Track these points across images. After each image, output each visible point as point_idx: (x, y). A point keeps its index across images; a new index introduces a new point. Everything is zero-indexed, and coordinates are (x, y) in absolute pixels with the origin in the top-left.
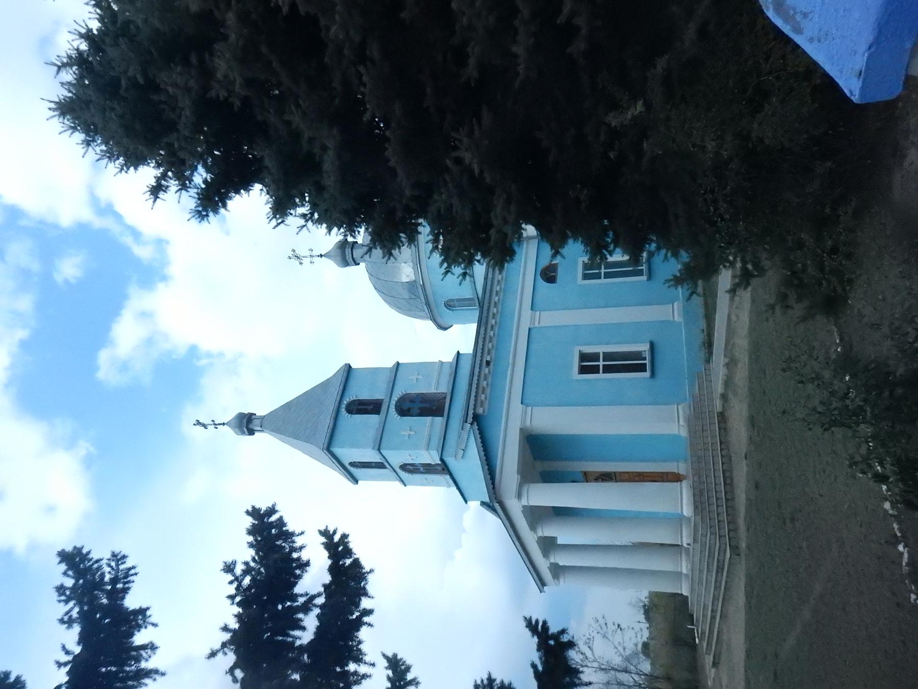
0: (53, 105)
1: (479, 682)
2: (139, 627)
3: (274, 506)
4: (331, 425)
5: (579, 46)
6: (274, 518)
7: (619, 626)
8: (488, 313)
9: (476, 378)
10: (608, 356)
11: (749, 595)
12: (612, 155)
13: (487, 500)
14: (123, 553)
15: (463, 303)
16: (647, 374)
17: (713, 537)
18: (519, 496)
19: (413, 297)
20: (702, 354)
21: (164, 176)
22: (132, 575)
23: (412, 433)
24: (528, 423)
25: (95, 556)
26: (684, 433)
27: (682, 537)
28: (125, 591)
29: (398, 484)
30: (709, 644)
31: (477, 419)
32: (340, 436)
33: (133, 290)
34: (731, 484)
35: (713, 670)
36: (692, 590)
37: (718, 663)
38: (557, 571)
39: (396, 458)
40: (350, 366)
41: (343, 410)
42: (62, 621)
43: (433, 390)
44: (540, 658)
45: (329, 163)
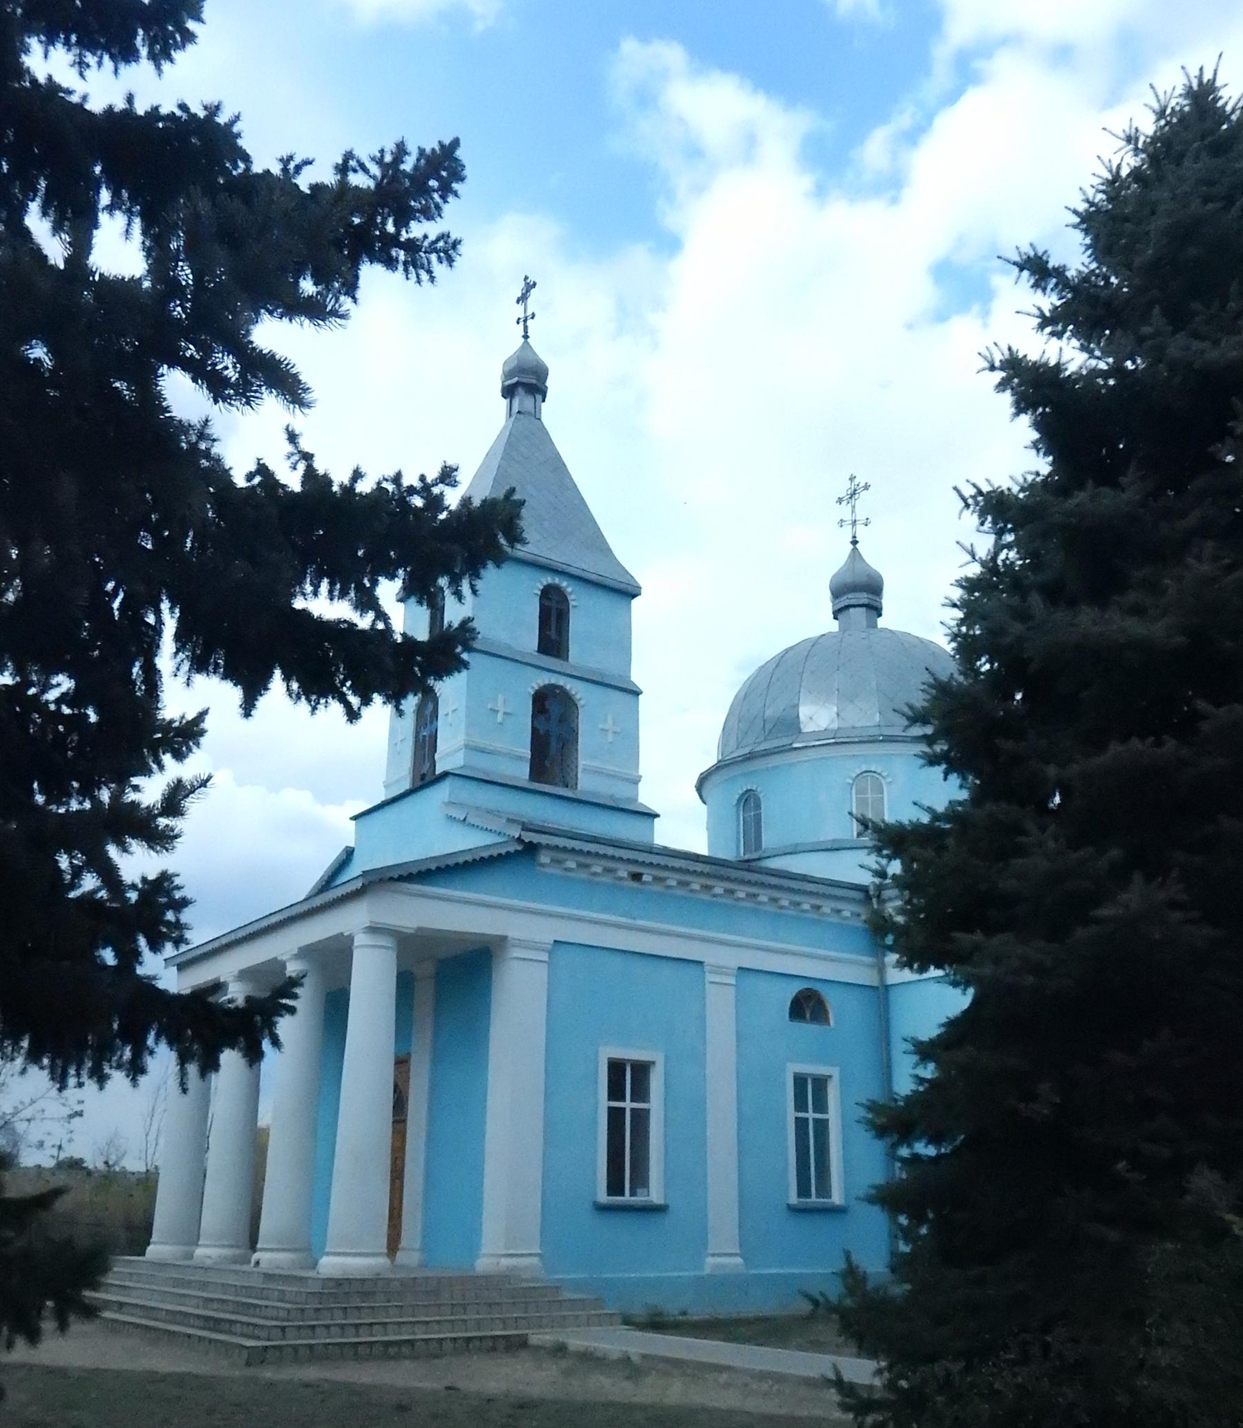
0: (1207, 76)
4: (570, 570)
7: (79, 1114)
8: (735, 880)
9: (610, 851)
10: (641, 1118)
14: (458, 258)
15: (753, 829)
16: (603, 1197)
17: (282, 1314)
18: (373, 930)
19: (768, 726)
20: (638, 1311)
22: (418, 276)
23: (500, 718)
25: (451, 208)
27: (271, 1250)
28: (390, 263)
36: (162, 1265)
40: (634, 596)
41: (548, 579)
42: (349, 156)
43: (583, 761)
45: (1111, 623)
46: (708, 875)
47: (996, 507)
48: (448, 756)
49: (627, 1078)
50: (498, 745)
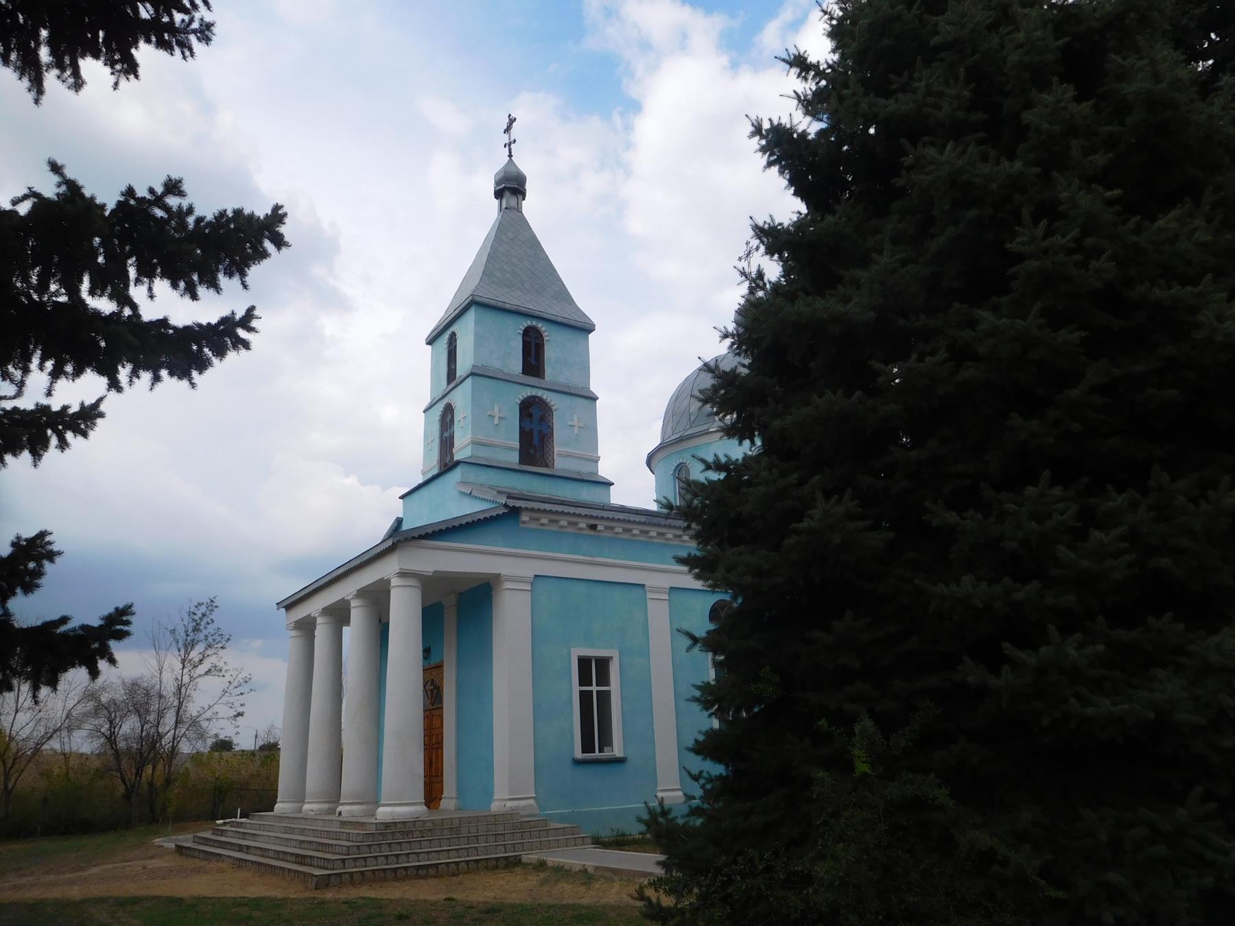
1: (48, 539)
2: (111, 63)
3: (287, 245)
4: (508, 306)
5: (972, 673)
6: (268, 245)
7: (240, 714)
9: (572, 510)
10: (604, 698)
11: (257, 903)
12: (823, 722)
13: (405, 527)
14: (214, 38)
16: (579, 754)
18: (403, 574)
19: (693, 418)
20: (605, 834)
21: (820, 74)
22: (183, 53)
23: (496, 421)
24: (508, 585)
26: (495, 807)
29: (427, 401)
30: (206, 841)
31: (513, 513)
32: (491, 318)
33: (718, 22)
34: (418, 877)
35: (172, 845)
36: (280, 818)
37: (181, 854)
38: (306, 627)
39: (462, 399)
40: (590, 331)
41: (528, 323)
43: (557, 449)
44: (74, 630)
46: (644, 524)
47: (772, 238)
48: (462, 449)
49: (593, 670)
50: (497, 441)
